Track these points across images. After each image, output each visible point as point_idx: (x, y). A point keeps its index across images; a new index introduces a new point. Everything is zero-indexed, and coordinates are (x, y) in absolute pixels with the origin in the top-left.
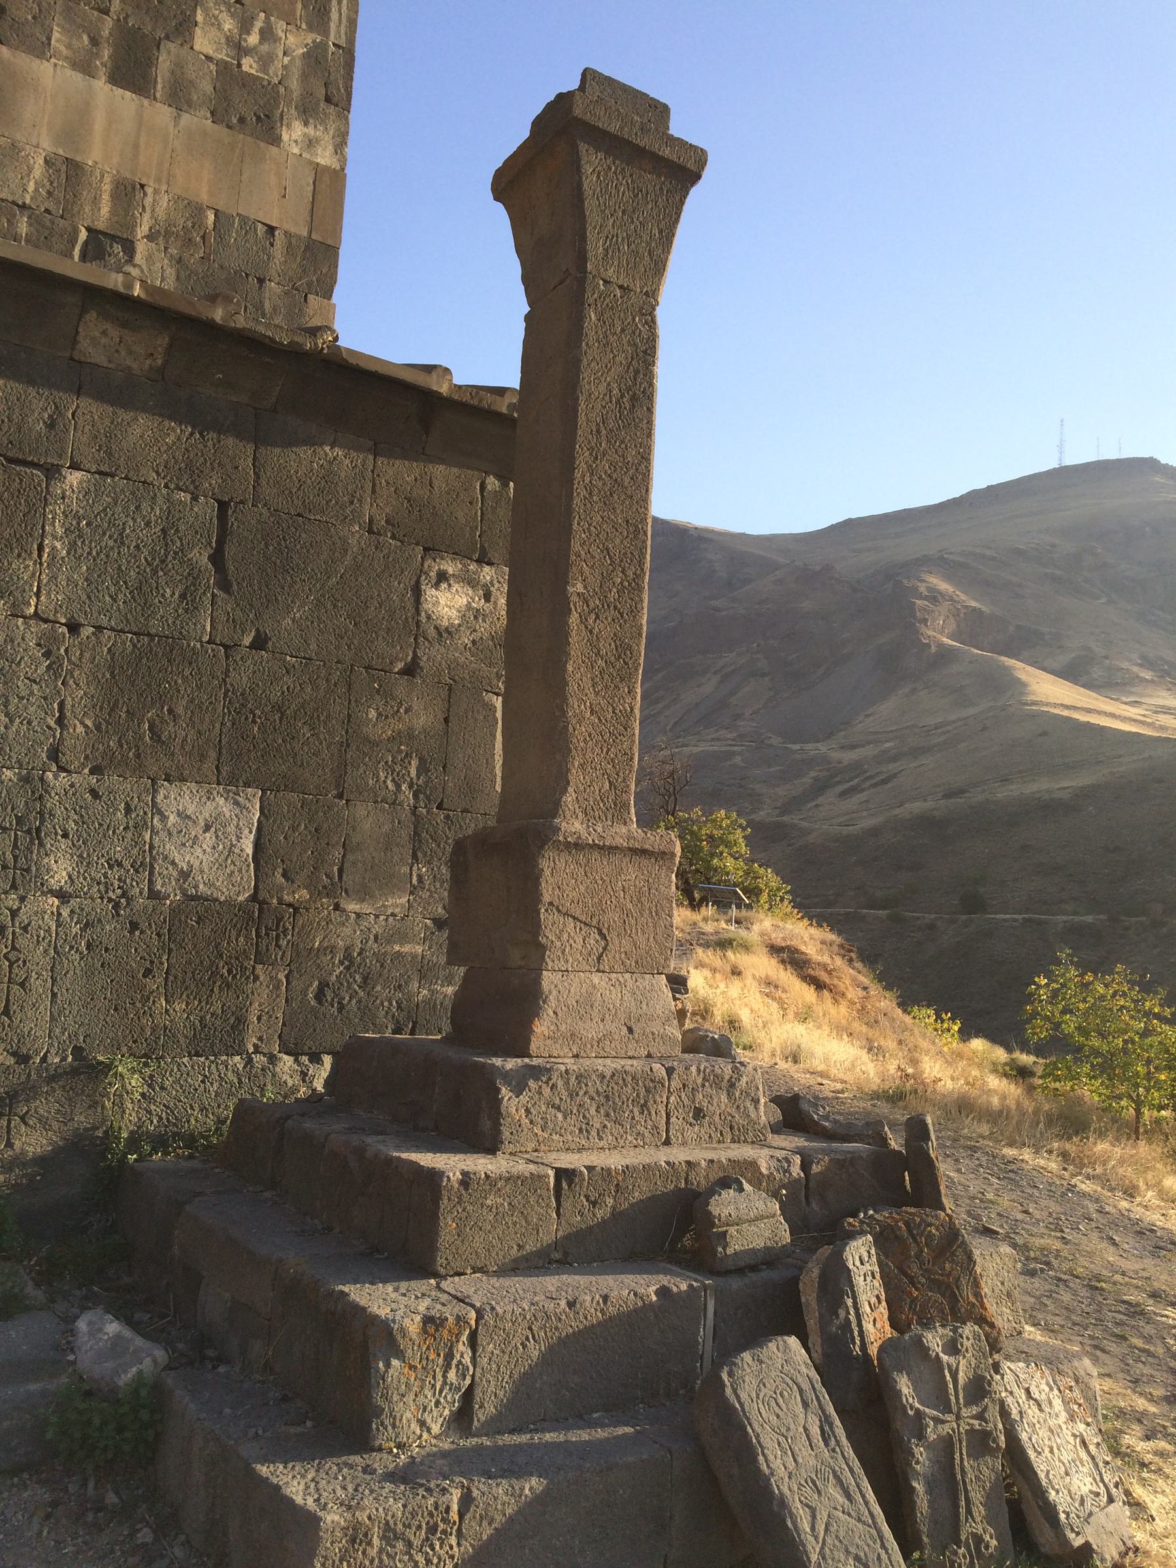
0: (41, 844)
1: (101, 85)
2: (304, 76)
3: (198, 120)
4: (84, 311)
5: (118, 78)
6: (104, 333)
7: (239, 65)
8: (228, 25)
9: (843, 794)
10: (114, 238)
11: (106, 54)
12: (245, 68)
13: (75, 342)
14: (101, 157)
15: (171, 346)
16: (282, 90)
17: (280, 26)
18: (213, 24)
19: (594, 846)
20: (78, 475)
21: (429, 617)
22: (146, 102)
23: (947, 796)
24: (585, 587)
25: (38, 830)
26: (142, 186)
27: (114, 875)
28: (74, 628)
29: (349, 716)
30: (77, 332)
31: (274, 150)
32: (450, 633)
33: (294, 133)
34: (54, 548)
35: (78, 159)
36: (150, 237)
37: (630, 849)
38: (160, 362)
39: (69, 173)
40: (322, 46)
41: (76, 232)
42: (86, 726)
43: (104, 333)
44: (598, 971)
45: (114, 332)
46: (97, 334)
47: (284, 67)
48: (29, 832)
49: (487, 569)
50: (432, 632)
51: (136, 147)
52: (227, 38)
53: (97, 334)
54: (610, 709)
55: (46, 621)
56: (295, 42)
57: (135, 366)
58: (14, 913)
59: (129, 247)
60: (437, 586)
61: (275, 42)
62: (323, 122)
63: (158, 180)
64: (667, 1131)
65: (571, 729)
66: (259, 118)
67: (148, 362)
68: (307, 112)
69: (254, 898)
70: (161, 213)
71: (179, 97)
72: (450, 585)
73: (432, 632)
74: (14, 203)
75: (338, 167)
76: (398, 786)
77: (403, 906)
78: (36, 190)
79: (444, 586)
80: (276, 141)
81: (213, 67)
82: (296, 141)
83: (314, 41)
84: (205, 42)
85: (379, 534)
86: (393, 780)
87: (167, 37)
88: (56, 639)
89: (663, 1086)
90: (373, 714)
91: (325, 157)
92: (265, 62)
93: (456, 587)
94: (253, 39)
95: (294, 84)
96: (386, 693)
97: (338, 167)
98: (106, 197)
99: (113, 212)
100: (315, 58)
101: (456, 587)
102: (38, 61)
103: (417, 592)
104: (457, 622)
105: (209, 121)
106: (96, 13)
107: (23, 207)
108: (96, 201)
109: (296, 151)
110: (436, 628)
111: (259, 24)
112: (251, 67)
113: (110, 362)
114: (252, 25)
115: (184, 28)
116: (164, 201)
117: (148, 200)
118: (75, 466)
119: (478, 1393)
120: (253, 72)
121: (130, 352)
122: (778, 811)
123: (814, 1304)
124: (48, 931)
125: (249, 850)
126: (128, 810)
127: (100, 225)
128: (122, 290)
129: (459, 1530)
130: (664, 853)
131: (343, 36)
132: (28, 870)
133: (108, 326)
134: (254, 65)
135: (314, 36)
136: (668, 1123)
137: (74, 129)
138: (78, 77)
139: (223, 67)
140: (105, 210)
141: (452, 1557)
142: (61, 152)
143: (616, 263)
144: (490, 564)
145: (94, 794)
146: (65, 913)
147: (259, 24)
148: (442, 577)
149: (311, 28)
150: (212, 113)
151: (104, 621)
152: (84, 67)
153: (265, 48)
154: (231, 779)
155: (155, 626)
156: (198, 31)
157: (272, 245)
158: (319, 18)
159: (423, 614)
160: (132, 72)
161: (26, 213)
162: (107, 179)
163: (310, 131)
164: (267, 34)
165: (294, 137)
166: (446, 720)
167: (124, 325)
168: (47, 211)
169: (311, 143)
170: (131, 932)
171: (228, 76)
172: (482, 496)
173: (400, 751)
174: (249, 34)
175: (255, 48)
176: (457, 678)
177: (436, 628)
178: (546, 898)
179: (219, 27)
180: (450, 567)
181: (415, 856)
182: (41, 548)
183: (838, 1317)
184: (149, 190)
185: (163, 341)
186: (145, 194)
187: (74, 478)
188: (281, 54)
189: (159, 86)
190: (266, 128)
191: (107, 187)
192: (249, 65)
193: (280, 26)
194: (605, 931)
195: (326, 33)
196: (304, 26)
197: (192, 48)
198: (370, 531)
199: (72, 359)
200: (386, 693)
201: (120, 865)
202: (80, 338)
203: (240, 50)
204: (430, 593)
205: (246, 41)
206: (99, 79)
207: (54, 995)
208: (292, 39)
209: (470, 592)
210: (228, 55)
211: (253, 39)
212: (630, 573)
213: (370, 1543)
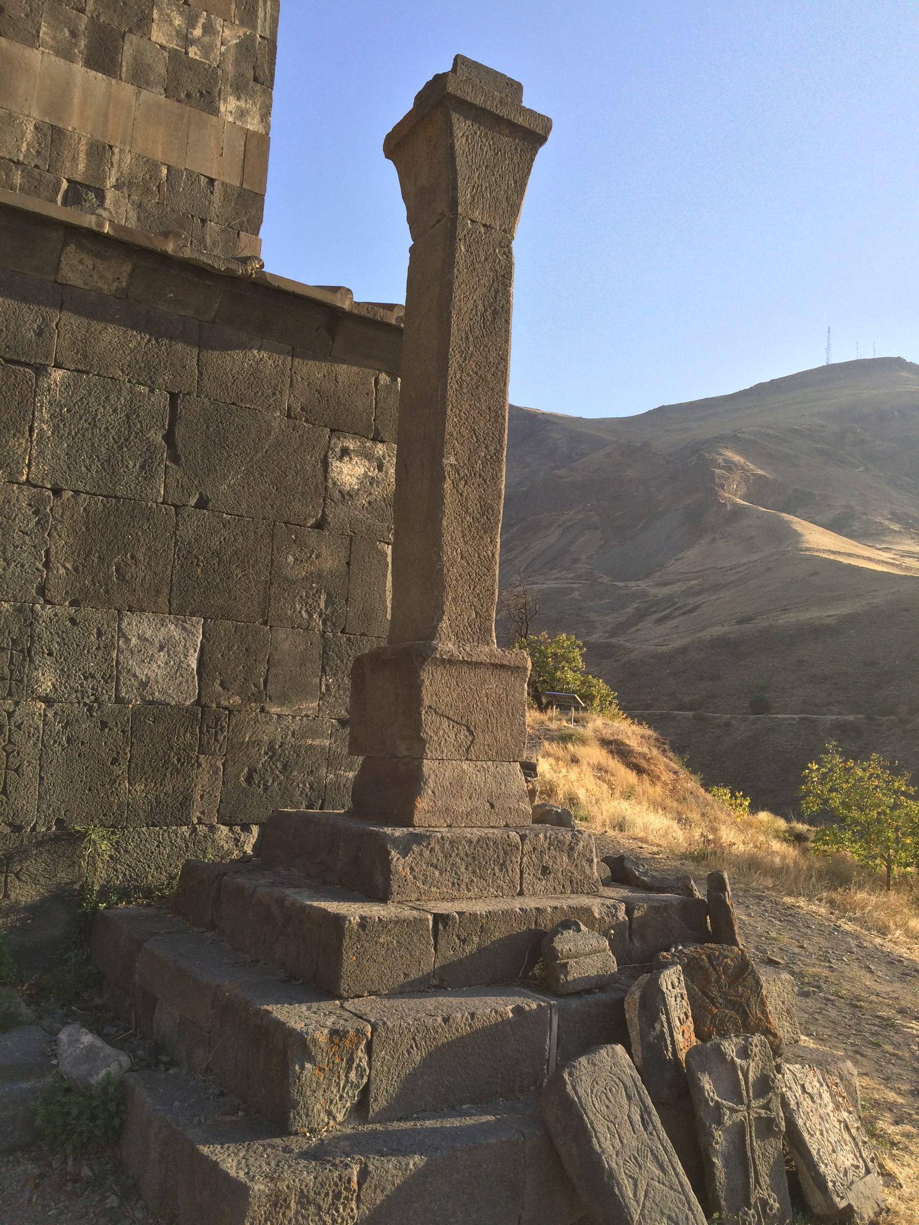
0: (31, 661)
1: (78, 68)
2: (237, 62)
3: (154, 96)
4: (65, 244)
5: (91, 63)
6: (81, 261)
7: (187, 53)
8: (178, 21)
9: (660, 621)
10: (88, 187)
11: (83, 43)
12: (191, 55)
13: (58, 269)
14: (78, 125)
15: (133, 271)
16: (220, 72)
17: (218, 23)
18: (166, 21)
19: (464, 662)
20: (61, 372)
21: (334, 484)
22: (114, 81)
23: (740, 622)
24: (457, 460)
25: (29, 650)
26: (111, 147)
27: (89, 684)
28: (57, 492)
29: (272, 560)
30: (60, 261)
31: (214, 119)
32: (351, 496)
33: (229, 106)
34: (41, 429)
35: (61, 125)
36: (117, 187)
37: (492, 664)
38: (124, 284)
39: (54, 136)
40: (252, 38)
41: (59, 183)
42: (66, 569)
43: (81, 261)
44: (467, 759)
45: (89, 262)
46: (75, 262)
47: (222, 54)
48: (22, 651)
49: (380, 445)
50: (337, 495)
51: (106, 115)
52: (177, 32)
53: (75, 262)
54: (476, 555)
55: (35, 486)
56: (230, 35)
57: (105, 287)
58: (10, 715)
59: (100, 195)
60: (341, 459)
61: (214, 34)
62: (252, 97)
63: (123, 142)
64: (521, 885)
65: (445, 571)
66: (201, 94)
67: (115, 284)
68: (239, 90)
69: (198, 702)
70: (125, 167)
71: (140, 77)
72: (351, 459)
73: (337, 495)
74: (11, 160)
75: (264, 133)
76: (311, 616)
77: (314, 709)
78: (28, 150)
79: (346, 459)
80: (215, 112)
81: (166, 54)
82: (231, 112)
83: (245, 34)
84: (158, 35)
85: (296, 418)
86: (307, 611)
87: (130, 31)
88: (43, 501)
89: (518, 849)
90: (291, 559)
91: (253, 124)
92: (207, 50)
93: (356, 459)
94: (197, 32)
95: (230, 68)
96: (301, 543)
97: (264, 133)
98: (82, 155)
99: (87, 167)
100: (246, 47)
101: (356, 459)
102: (29, 50)
103: (326, 464)
104: (356, 487)
105: (163, 97)
106: (74, 12)
107: (18, 163)
108: (74, 159)
109: (231, 119)
110: (340, 491)
111: (202, 21)
112: (195, 54)
113: (86, 284)
114: (197, 21)
115: (143, 24)
116: (128, 159)
117: (116, 158)
118: (58, 366)
119: (373, 1087)
120: (197, 57)
121: (101, 277)
122: (607, 635)
123: (636, 1020)
124: (37, 729)
125: (194, 666)
126: (100, 634)
127: (78, 178)
128: (95, 228)
129: (358, 1196)
130: (518, 667)
131: (268, 30)
132: (21, 681)
133: (84, 256)
134: (198, 53)
135: (245, 29)
136: (521, 878)
137: (58, 101)
138: (61, 62)
139: (174, 54)
140: (81, 166)
141: (353, 1218)
142: (47, 120)
143: (481, 206)
144: (382, 442)
145: (73, 621)
146: (50, 715)
147: (202, 21)
148: (345, 452)
149: (242, 24)
150: (165, 90)
151: (80, 486)
152: (66, 54)
153: (206, 39)
154: (181, 611)
155: (120, 490)
156: (154, 26)
157: (212, 193)
158: (249, 16)
159: (330, 481)
160: (103, 57)
161: (20, 168)
162: (84, 141)
163: (242, 104)
164: (208, 29)
165: (229, 109)
166: (348, 564)
167: (97, 255)
168: (36, 166)
169: (242, 114)
170: (102, 730)
171: (178, 61)
172: (376, 389)
173: (312, 588)
174: (194, 28)
175: (199, 39)
176: (356, 531)
177: (340, 491)
178: (426, 702)
179: (171, 23)
180: (351, 445)
181: (323, 670)
182: (31, 430)
183: (654, 1029)
184: (116, 150)
185: (127, 268)
186: (113, 153)
187: (58, 375)
188: (219, 44)
189: (124, 69)
190: (208, 102)
191: (83, 148)
192: (194, 52)
193: (218, 23)
194: (472, 728)
195: (254, 28)
196: (237, 22)
197: (149, 39)
198: (289, 416)
199: (56, 282)
200: (301, 543)
201: (93, 677)
202: (62, 266)
203: (187, 41)
204: (336, 464)
205: (192, 34)
206: (77, 63)
207: (41, 779)
208: (227, 32)
209: (367, 464)
210: (178, 45)
211: (197, 32)
212: (492, 449)
213: (288, 1207)
